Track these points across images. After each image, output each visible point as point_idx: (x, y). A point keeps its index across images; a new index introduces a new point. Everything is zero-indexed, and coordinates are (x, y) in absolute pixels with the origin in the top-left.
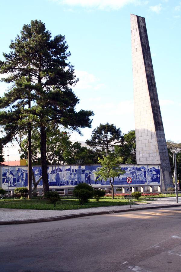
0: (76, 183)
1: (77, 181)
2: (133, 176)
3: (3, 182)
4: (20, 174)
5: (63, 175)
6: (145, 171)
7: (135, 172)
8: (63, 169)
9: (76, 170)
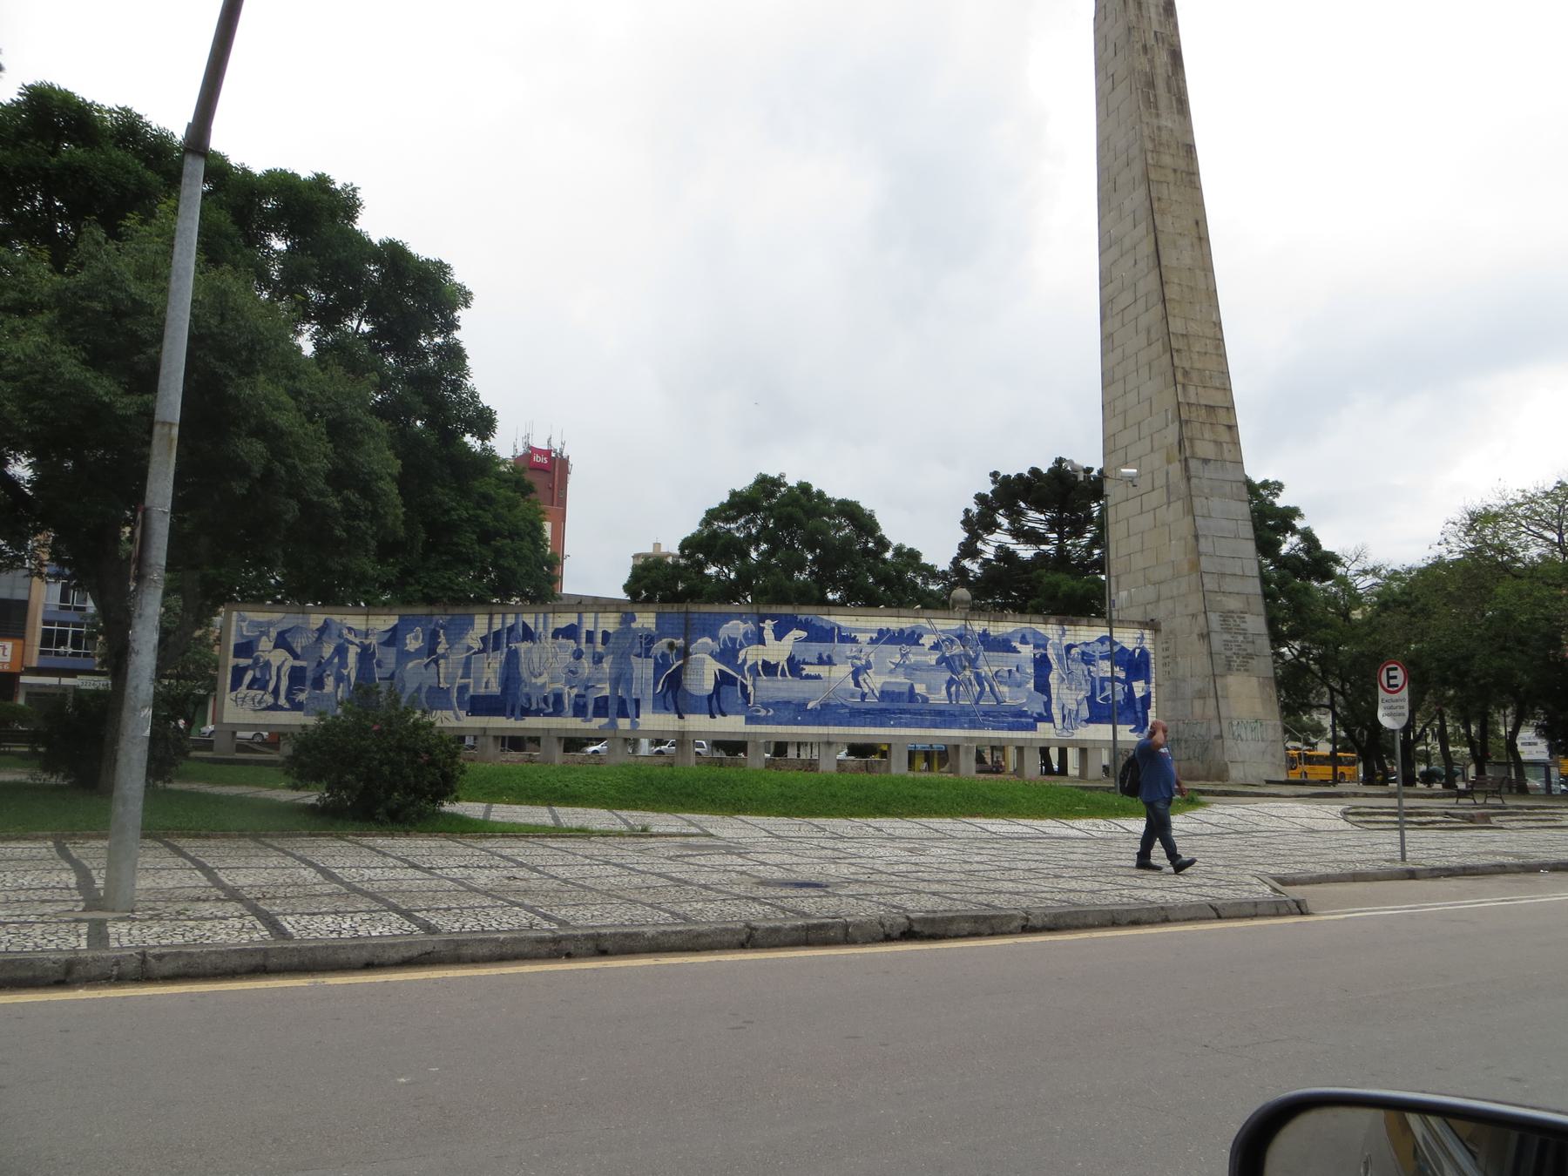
1: (607, 692)
2: (959, 684)
3: (236, 684)
4: (328, 650)
5: (536, 660)
6: (1045, 657)
7: (973, 662)
8: (541, 629)
9: (606, 635)
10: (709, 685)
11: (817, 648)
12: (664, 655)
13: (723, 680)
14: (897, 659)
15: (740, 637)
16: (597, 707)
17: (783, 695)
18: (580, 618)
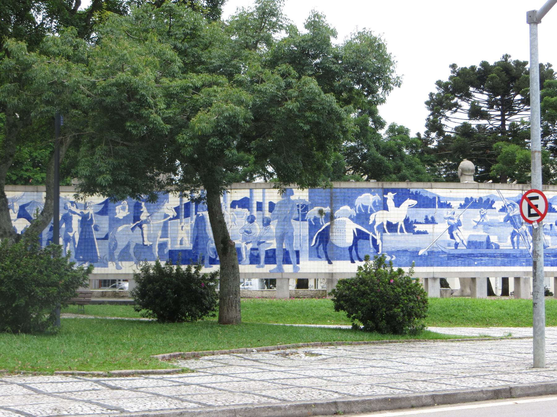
0: (270, 254)
1: (274, 246)
2: (519, 235)
10: (349, 240)
11: (425, 212)
12: (315, 219)
13: (360, 236)
14: (478, 218)
15: (370, 205)
16: (267, 256)
17: (402, 246)
18: (251, 193)
